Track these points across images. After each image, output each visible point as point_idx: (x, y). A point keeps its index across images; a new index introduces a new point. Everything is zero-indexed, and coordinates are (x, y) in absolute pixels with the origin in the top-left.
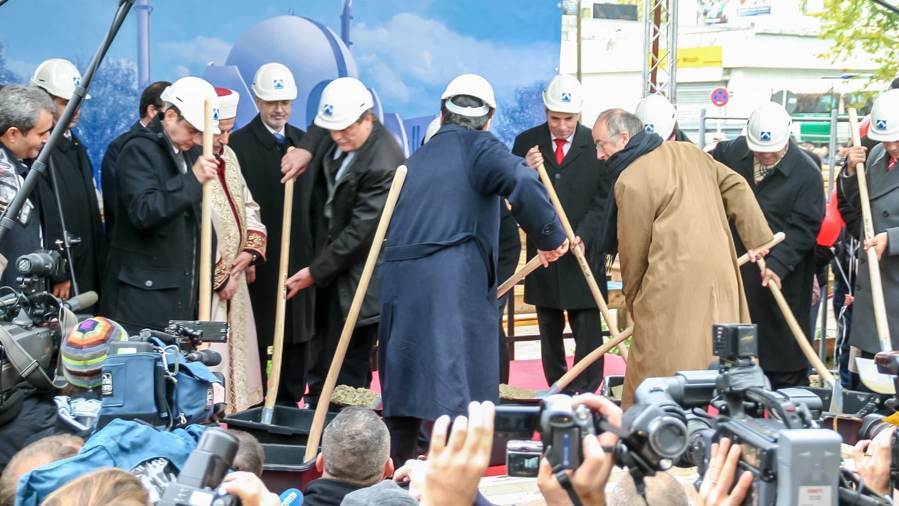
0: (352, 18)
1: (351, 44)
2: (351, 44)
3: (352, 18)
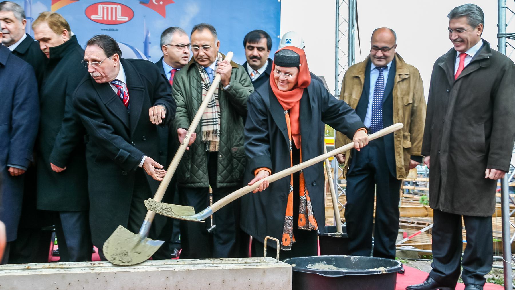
0: (150, 43)
1: (150, 57)
2: (150, 57)
3: (150, 43)
